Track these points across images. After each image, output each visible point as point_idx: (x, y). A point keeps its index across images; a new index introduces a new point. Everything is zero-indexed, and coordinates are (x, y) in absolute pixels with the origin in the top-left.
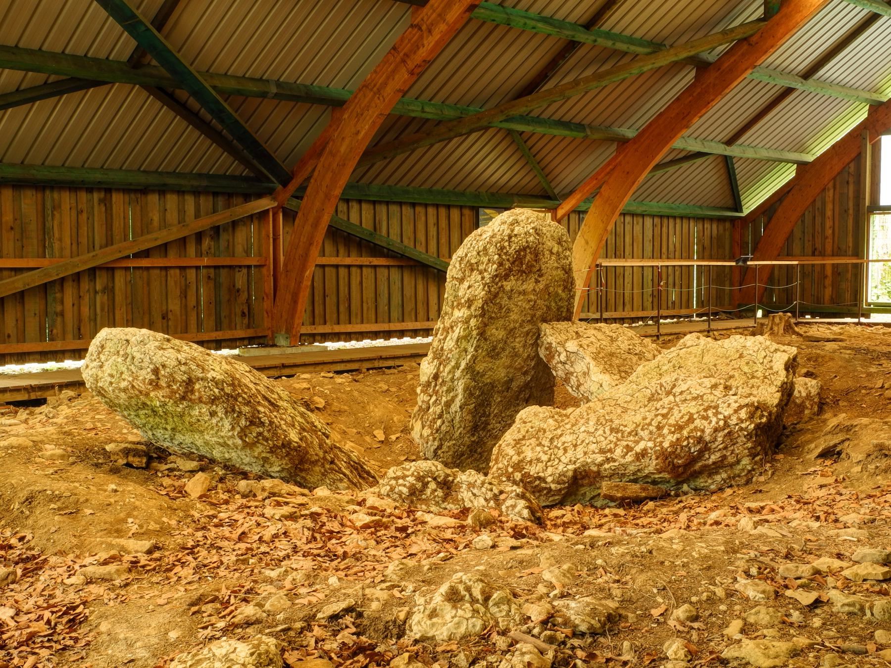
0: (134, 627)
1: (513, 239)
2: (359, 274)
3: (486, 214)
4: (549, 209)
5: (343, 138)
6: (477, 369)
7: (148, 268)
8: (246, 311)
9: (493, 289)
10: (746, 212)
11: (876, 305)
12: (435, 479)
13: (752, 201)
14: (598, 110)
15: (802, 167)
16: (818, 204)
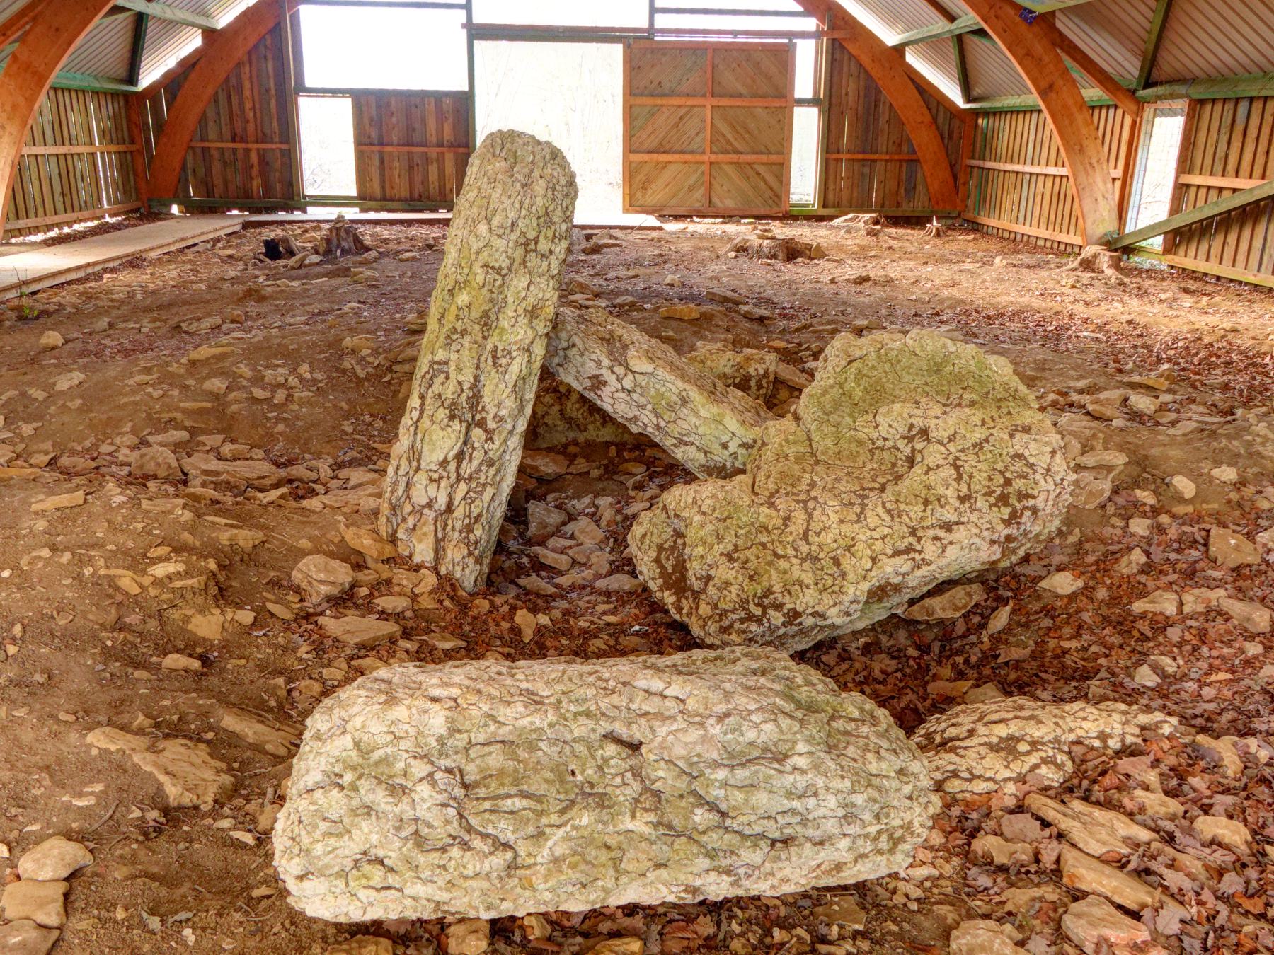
0: (78, 951)
13: (149, 76)
14: (1211, 28)
15: (210, 34)
16: (233, 81)
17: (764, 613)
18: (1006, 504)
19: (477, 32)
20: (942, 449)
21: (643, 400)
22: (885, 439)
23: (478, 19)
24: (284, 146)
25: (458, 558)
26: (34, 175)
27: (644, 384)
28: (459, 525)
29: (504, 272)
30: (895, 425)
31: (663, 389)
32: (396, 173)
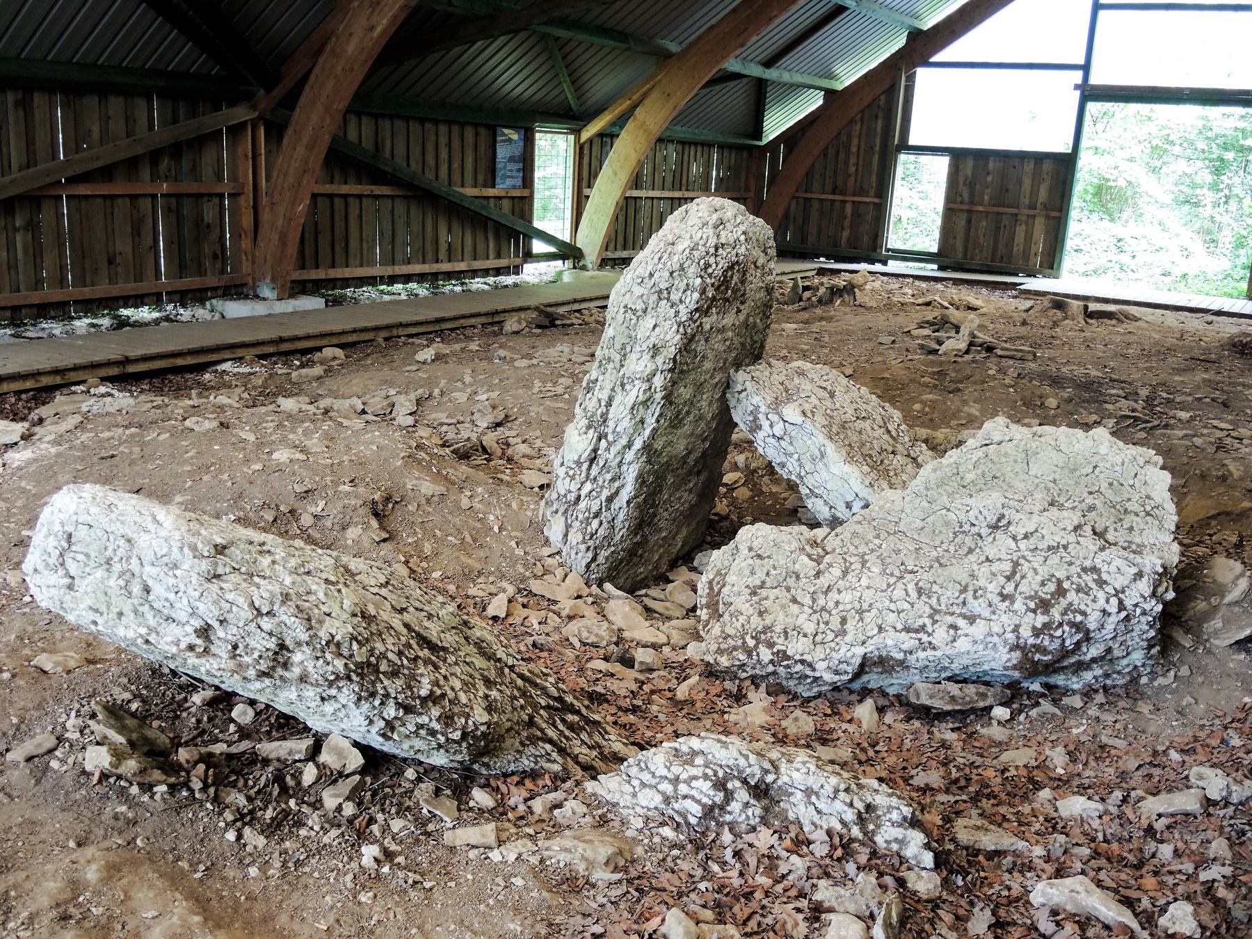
1: (720, 251)
3: (504, 135)
4: (572, 131)
5: (351, 34)
6: (656, 446)
7: (86, 197)
9: (689, 331)
10: (765, 141)
11: (894, 251)
12: (745, 782)
15: (830, 94)
16: (844, 138)
17: (756, 646)
18: (1046, 612)
19: (1090, 94)
20: (1013, 545)
21: (790, 449)
23: (1094, 80)
24: (877, 200)
25: (574, 543)
27: (793, 434)
29: (639, 313)
30: (985, 512)
31: (809, 442)
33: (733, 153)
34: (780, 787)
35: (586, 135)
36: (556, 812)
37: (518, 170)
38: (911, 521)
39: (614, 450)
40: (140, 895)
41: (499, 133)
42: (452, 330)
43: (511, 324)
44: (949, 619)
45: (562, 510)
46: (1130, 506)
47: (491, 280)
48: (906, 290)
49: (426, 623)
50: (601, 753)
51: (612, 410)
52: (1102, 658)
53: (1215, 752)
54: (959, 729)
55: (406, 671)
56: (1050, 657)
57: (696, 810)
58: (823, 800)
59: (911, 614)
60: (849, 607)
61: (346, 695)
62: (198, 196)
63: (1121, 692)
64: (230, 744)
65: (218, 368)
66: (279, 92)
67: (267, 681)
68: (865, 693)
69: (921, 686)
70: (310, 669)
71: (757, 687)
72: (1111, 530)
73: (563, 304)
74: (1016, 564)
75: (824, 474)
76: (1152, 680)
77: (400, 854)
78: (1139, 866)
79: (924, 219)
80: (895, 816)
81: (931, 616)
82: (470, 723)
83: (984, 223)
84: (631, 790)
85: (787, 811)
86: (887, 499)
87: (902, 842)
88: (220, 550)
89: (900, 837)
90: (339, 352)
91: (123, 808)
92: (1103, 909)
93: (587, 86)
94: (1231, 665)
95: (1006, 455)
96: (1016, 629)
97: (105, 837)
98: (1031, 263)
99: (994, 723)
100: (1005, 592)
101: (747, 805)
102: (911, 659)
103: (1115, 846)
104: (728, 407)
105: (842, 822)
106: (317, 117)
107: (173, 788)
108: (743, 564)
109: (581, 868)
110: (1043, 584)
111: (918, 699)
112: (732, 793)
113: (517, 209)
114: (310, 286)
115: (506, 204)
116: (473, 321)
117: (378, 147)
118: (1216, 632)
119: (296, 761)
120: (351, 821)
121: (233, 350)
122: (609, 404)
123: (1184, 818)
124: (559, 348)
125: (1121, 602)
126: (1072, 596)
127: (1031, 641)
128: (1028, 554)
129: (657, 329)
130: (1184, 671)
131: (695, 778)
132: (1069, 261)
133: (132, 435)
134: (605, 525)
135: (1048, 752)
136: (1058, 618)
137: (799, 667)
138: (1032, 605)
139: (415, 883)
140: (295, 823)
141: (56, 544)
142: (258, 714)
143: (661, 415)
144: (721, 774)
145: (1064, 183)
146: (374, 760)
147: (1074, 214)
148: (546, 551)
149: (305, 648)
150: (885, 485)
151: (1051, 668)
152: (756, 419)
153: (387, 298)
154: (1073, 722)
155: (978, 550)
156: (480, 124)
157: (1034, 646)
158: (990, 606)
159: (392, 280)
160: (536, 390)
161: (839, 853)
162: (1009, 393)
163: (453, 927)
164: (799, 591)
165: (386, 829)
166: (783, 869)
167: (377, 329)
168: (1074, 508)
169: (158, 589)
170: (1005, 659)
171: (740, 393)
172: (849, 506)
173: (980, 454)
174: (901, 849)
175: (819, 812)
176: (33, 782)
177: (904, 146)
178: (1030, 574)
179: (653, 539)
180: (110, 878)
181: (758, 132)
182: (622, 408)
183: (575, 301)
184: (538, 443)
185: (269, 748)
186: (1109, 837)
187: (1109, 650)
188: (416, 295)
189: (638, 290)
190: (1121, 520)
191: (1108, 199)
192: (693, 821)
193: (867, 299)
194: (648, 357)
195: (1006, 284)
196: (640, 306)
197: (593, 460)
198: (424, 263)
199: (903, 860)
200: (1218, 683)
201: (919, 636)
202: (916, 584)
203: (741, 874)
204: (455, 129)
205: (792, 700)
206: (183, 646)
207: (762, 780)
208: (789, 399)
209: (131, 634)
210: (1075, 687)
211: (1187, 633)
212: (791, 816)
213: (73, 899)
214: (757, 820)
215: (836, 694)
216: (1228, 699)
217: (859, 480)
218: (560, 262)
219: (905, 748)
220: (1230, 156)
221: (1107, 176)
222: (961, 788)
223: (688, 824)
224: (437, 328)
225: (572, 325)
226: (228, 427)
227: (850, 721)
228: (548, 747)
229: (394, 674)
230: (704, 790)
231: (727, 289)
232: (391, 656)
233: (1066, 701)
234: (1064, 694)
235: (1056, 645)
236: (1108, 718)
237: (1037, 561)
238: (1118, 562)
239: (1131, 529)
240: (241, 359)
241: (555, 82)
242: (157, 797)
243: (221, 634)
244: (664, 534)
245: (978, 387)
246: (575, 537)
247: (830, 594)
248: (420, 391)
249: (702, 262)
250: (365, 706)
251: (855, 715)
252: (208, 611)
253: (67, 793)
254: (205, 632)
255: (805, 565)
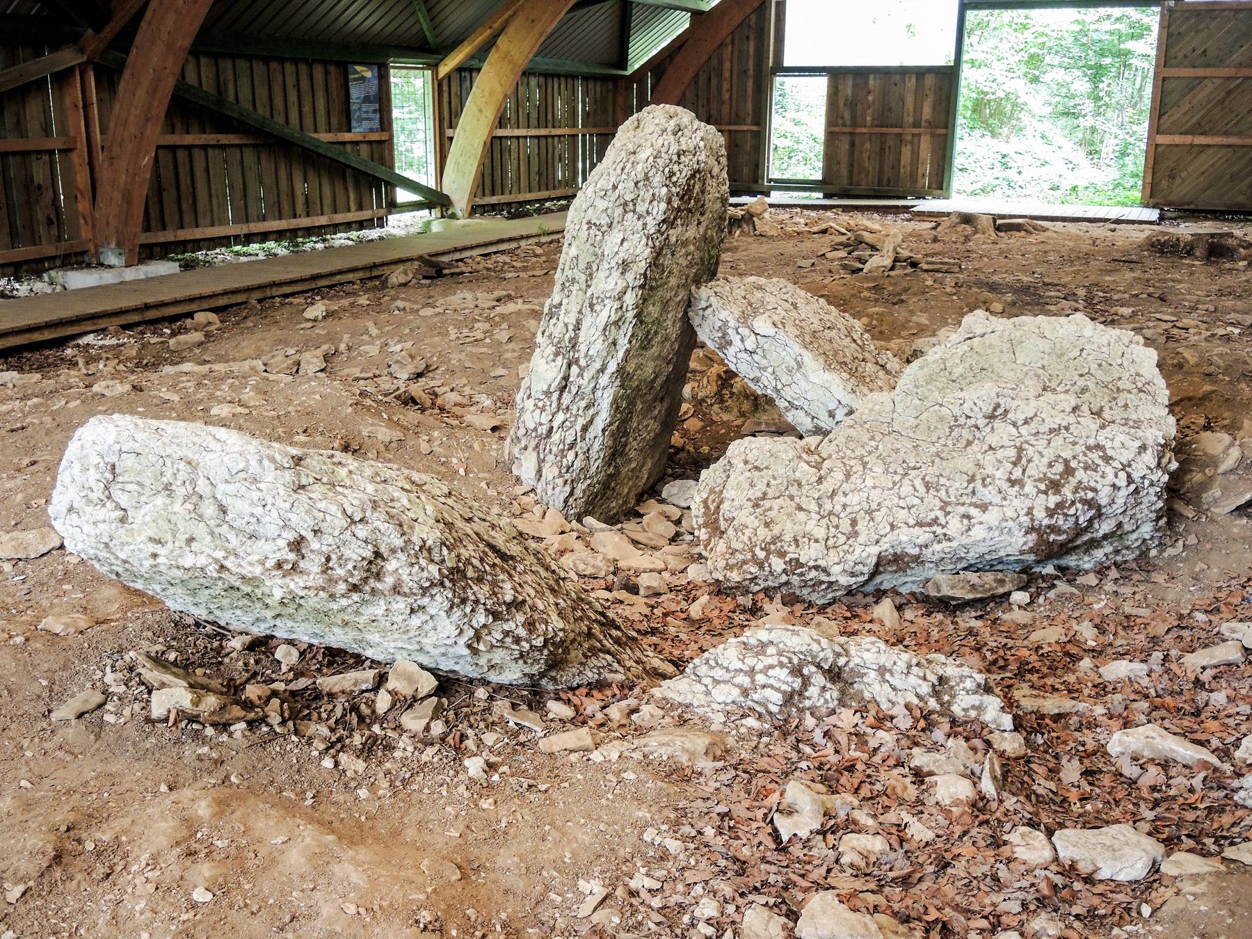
2: (203, 158)
3: (357, 72)
8: (53, 216)
9: (657, 244)
10: (630, 71)
11: (776, 181)
12: (819, 666)
16: (715, 62)
17: (767, 558)
18: (1058, 492)
20: (1014, 431)
21: (764, 363)
22: (968, 417)
24: (755, 128)
25: (550, 477)
26: (514, 155)
27: (766, 347)
28: (555, 449)
30: (980, 403)
31: (784, 354)
32: (866, 155)
33: (599, 84)
34: (852, 670)
35: (444, 70)
36: (634, 717)
37: (374, 112)
38: (904, 420)
39: (587, 375)
40: (260, 825)
41: (350, 70)
42: (330, 287)
43: (397, 276)
44: (961, 510)
45: (533, 444)
46: (1121, 384)
47: (354, 234)
48: (797, 219)
49: (492, 533)
50: (644, 669)
51: (582, 334)
52: (1113, 534)
53: (1239, 609)
54: (981, 617)
55: (489, 578)
56: (1064, 536)
57: (777, 698)
58: (897, 676)
59: (922, 508)
60: (857, 508)
61: (438, 603)
62: (26, 154)
63: (1134, 565)
64: (288, 682)
65: (80, 342)
66: (108, 32)
67: (356, 597)
68: (879, 595)
69: (940, 577)
70: (405, 577)
71: (771, 599)
72: (1106, 409)
73: (444, 253)
74: (1020, 450)
75: (803, 384)
76: (1161, 552)
77: (502, 764)
78: (1197, 713)
79: (801, 147)
80: (969, 684)
81: (942, 509)
82: (550, 629)
83: (868, 145)
84: (704, 688)
85: (862, 691)
86: (874, 403)
87: (979, 708)
88: (298, 461)
89: (977, 703)
90: (212, 317)
91: (206, 749)
92: (1181, 750)
93: (442, 16)
94: (1235, 530)
95: (991, 346)
96: (1030, 512)
97: (195, 779)
98: (919, 184)
99: (1015, 607)
100: (1013, 478)
101: (824, 689)
102: (927, 553)
103: (1168, 699)
104: (692, 327)
105: (917, 695)
106: (157, 60)
107: (251, 724)
108: (741, 478)
109: (684, 759)
110: (1050, 465)
111: (939, 591)
112: (808, 678)
113: (376, 156)
114: (157, 249)
115: (364, 149)
116: (350, 276)
117: (220, 88)
118: (1215, 501)
119: (363, 692)
120: (443, 740)
121: (95, 320)
122: (577, 327)
123: (1227, 668)
124: (459, 295)
125: (1129, 476)
126: (1080, 475)
127: (1046, 522)
128: (1031, 439)
129: (625, 244)
130: (1192, 540)
131: (771, 667)
132: (958, 181)
133: (35, 406)
134: (581, 456)
135: (1076, 628)
136: (1070, 496)
137: (813, 574)
138: (1043, 487)
139: (530, 786)
140: (385, 747)
141: (99, 476)
142: (302, 654)
143: (632, 335)
144: (795, 661)
145: (948, 98)
146: (447, 685)
147: (959, 132)
148: (519, 490)
149: (400, 554)
150: (866, 390)
151: (1066, 549)
152: (725, 335)
153: (243, 259)
154: (1091, 599)
155: (976, 442)
156: (330, 62)
157: (1049, 527)
158: (1000, 492)
159: (248, 239)
160: (453, 337)
161: (922, 723)
162: (953, 301)
163: (583, 821)
164: (803, 498)
165: (480, 742)
166: (873, 743)
167: (249, 290)
168: (1067, 392)
169: (238, 508)
170: (1021, 543)
171: (704, 309)
172: (831, 414)
173: (965, 347)
174: (979, 715)
175: (894, 689)
176: (92, 737)
177: (780, 68)
178: (1036, 458)
179: (624, 470)
180: (223, 812)
181: (622, 61)
182: (593, 330)
183: (456, 250)
184: (467, 391)
185: (329, 682)
186: (1161, 692)
187: (1120, 525)
188: (276, 255)
189: (601, 204)
190: (1115, 399)
191: (994, 115)
192: (774, 709)
193: (767, 228)
194: (618, 274)
195: (897, 207)
196: (604, 221)
197: (562, 389)
198: (280, 219)
199: (984, 726)
200: (1227, 549)
201: (933, 529)
202: (923, 479)
203: (837, 752)
204: (303, 68)
205: (808, 608)
206: (270, 563)
207: (834, 664)
208: (756, 312)
209: (202, 561)
210: (1087, 566)
211: (1187, 504)
212: (867, 696)
213: (191, 836)
214: (836, 702)
215: (851, 599)
216: (1239, 561)
217: (841, 387)
218: (427, 211)
219: (932, 640)
220: (1107, 61)
221: (986, 89)
222: (1000, 668)
223: (770, 713)
224: (313, 286)
225: (462, 273)
226: (142, 390)
227: (871, 621)
228: (609, 657)
229: (479, 580)
230: (782, 677)
231: (690, 199)
232: (476, 562)
233: (1080, 580)
234: (1077, 574)
235: (1070, 523)
236: (1126, 590)
237: (1041, 444)
238: (1121, 438)
239: (1126, 406)
240: (104, 330)
241: (409, 10)
242: (238, 735)
243: (315, 545)
244: (633, 465)
245: (922, 297)
246: (550, 472)
247: (836, 498)
248: (325, 347)
249: (667, 170)
250: (457, 613)
251: (875, 616)
252: (301, 522)
253: (134, 744)
254: (297, 545)
255: (805, 471)
